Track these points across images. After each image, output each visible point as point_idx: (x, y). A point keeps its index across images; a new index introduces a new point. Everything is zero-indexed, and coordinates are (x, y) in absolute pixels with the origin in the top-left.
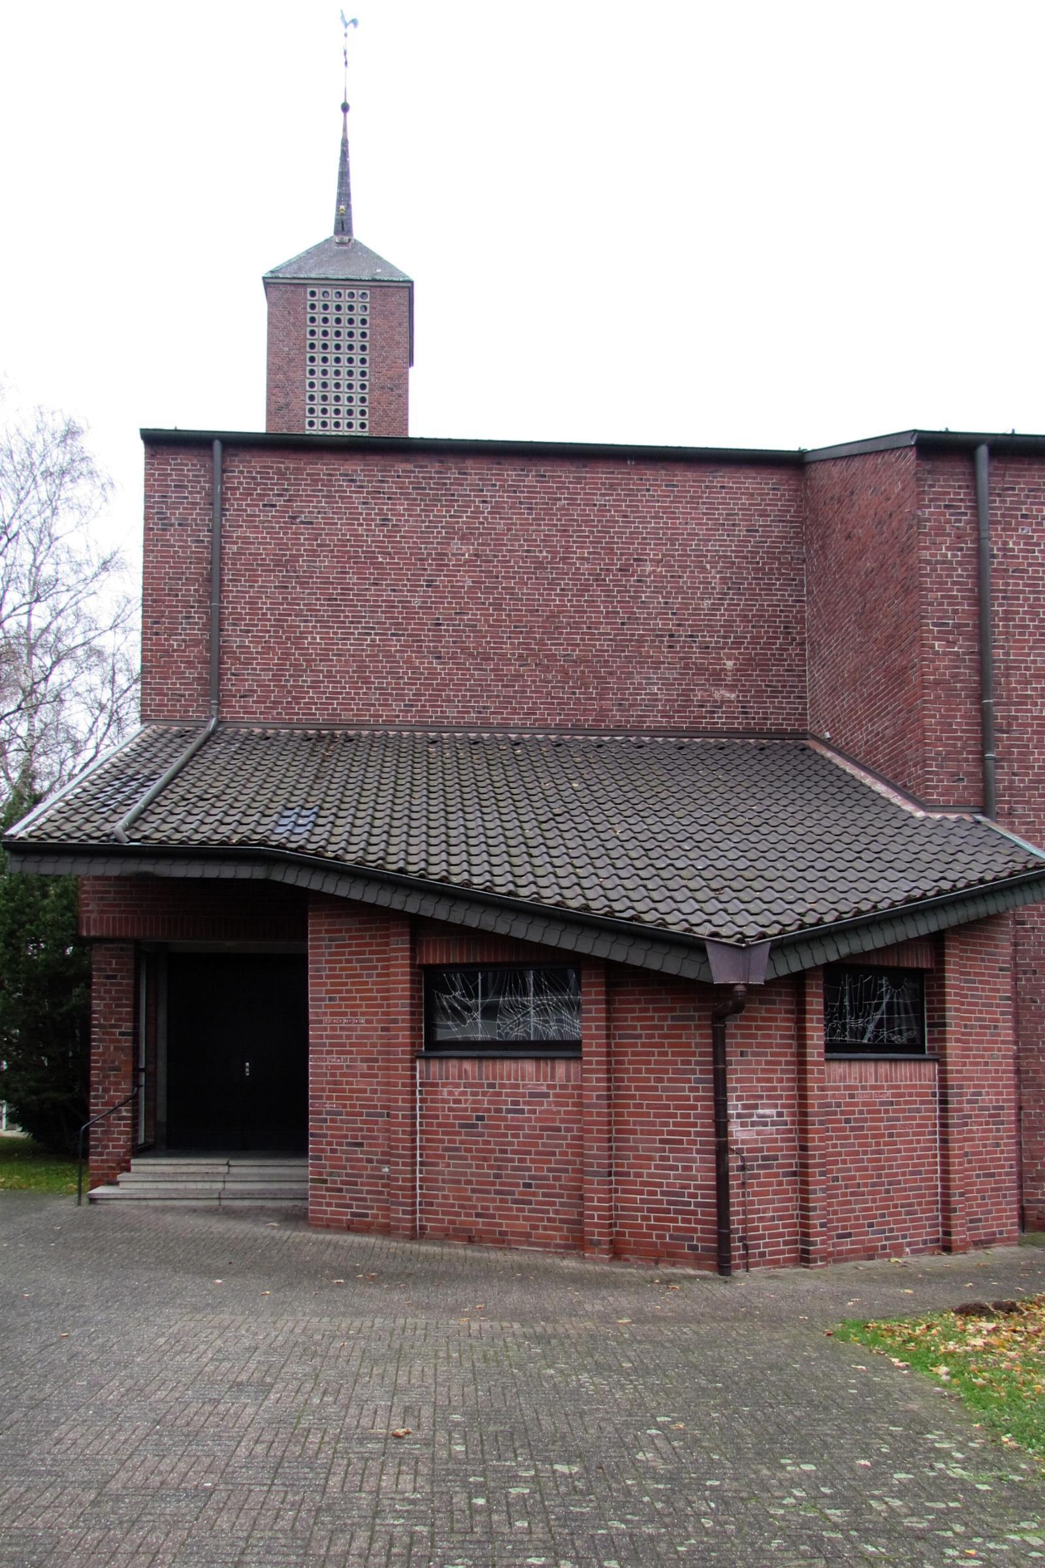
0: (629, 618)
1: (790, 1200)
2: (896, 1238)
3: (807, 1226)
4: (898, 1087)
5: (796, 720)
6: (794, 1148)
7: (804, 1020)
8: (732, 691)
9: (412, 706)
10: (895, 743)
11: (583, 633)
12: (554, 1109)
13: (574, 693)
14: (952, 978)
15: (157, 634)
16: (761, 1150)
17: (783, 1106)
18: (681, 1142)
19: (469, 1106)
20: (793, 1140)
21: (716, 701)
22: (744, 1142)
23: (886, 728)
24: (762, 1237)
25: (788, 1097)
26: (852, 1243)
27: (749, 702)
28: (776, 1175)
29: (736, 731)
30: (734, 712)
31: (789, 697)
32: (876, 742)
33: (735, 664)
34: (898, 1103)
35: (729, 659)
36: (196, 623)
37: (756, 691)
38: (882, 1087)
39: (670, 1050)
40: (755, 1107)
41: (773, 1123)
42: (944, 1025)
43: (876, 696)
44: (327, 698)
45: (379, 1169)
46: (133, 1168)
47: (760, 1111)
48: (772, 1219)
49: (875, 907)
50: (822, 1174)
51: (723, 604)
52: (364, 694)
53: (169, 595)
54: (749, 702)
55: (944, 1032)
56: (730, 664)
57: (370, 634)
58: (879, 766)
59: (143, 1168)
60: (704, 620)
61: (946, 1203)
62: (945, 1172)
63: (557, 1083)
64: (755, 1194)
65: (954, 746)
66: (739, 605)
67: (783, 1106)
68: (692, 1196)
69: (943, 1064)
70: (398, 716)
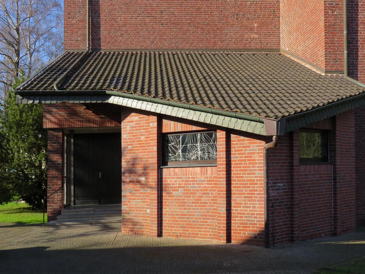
0: (224, 9)
1: (287, 218)
2: (319, 230)
3: (293, 228)
4: (321, 174)
5: (277, 44)
6: (288, 198)
7: (292, 150)
8: (256, 35)
9: (153, 42)
10: (313, 49)
11: (209, 15)
12: (207, 186)
13: (206, 36)
14: (338, 133)
15: (69, 18)
16: (278, 199)
17: (286, 182)
18: (252, 197)
19: (177, 186)
20: (288, 195)
21: (251, 38)
22: (273, 197)
23: (310, 44)
24: (278, 232)
25: (287, 179)
26: (306, 233)
27: (262, 38)
28: (283, 209)
29: (258, 49)
30: (257, 42)
31: (275, 36)
32: (306, 49)
33: (257, 25)
34: (321, 180)
35: (255, 23)
36: (82, 14)
37: (264, 35)
38: (316, 174)
39: (248, 162)
40: (276, 183)
41: (283, 189)
42: (335, 151)
43: (307, 33)
44: (126, 40)
45: (146, 211)
46: (62, 214)
47: (278, 185)
48: (281, 225)
49: (318, 105)
50: (298, 207)
51: (254, 3)
52: (138, 38)
53: (73, 4)
54: (262, 38)
55: (335, 153)
56: (256, 25)
57: (139, 16)
58: (307, 58)
59: (66, 213)
60: (248, 9)
61: (335, 217)
62: (335, 205)
63: (208, 176)
64: (276, 216)
65: (335, 49)
66: (259, 3)
67: (286, 182)
68: (255, 218)
69: (335, 165)
70: (149, 46)
